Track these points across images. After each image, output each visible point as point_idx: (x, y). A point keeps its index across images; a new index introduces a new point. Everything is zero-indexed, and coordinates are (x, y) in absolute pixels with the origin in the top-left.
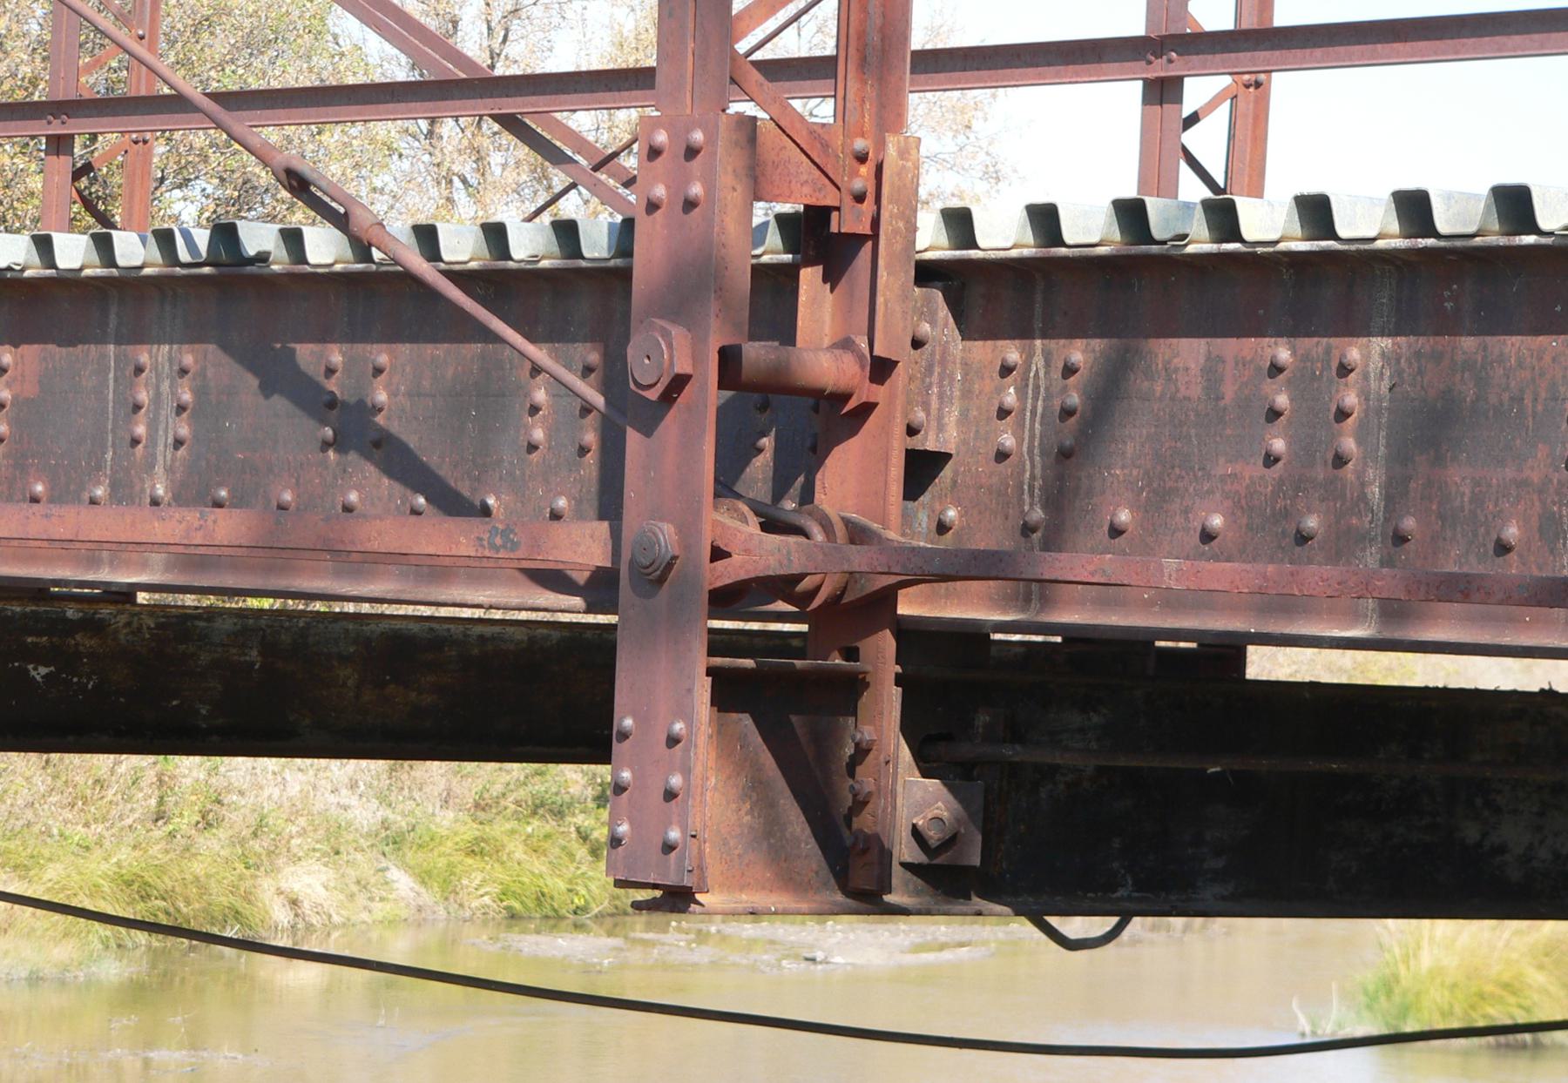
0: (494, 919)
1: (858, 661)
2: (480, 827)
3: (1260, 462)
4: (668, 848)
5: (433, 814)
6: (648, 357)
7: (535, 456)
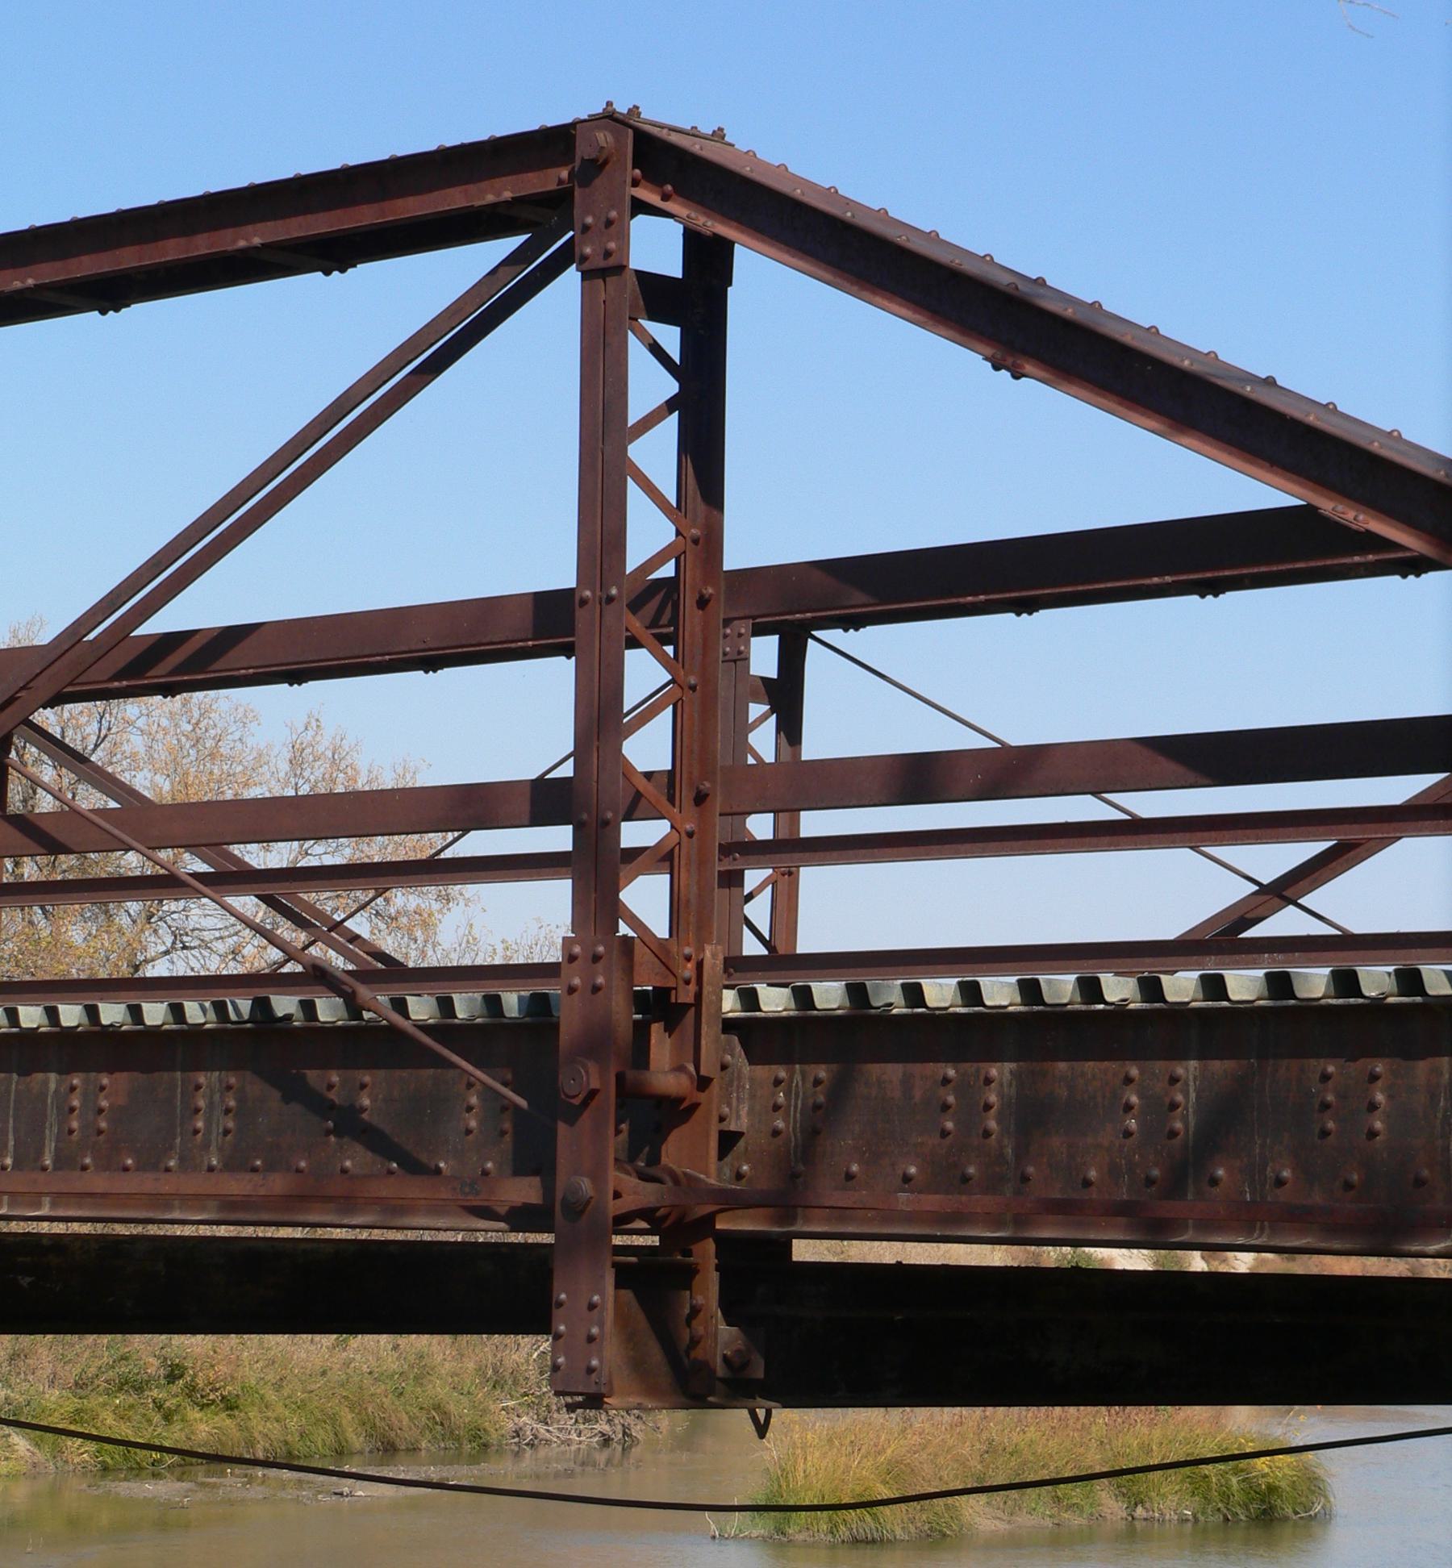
0: (91, 1471)
1: (691, 1256)
2: (80, 1401)
3: (938, 1135)
4: (591, 1370)
5: (44, 1393)
7: (470, 1137)
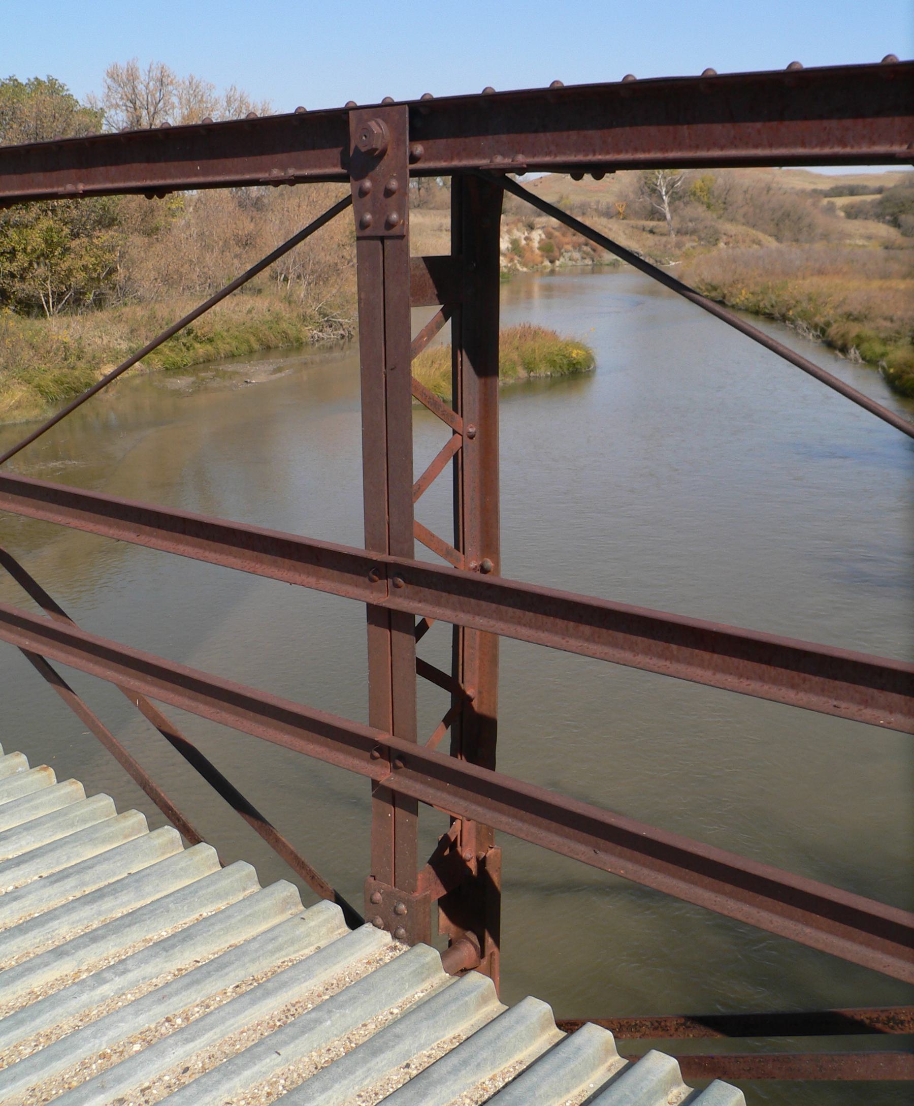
6: (366, 136)
